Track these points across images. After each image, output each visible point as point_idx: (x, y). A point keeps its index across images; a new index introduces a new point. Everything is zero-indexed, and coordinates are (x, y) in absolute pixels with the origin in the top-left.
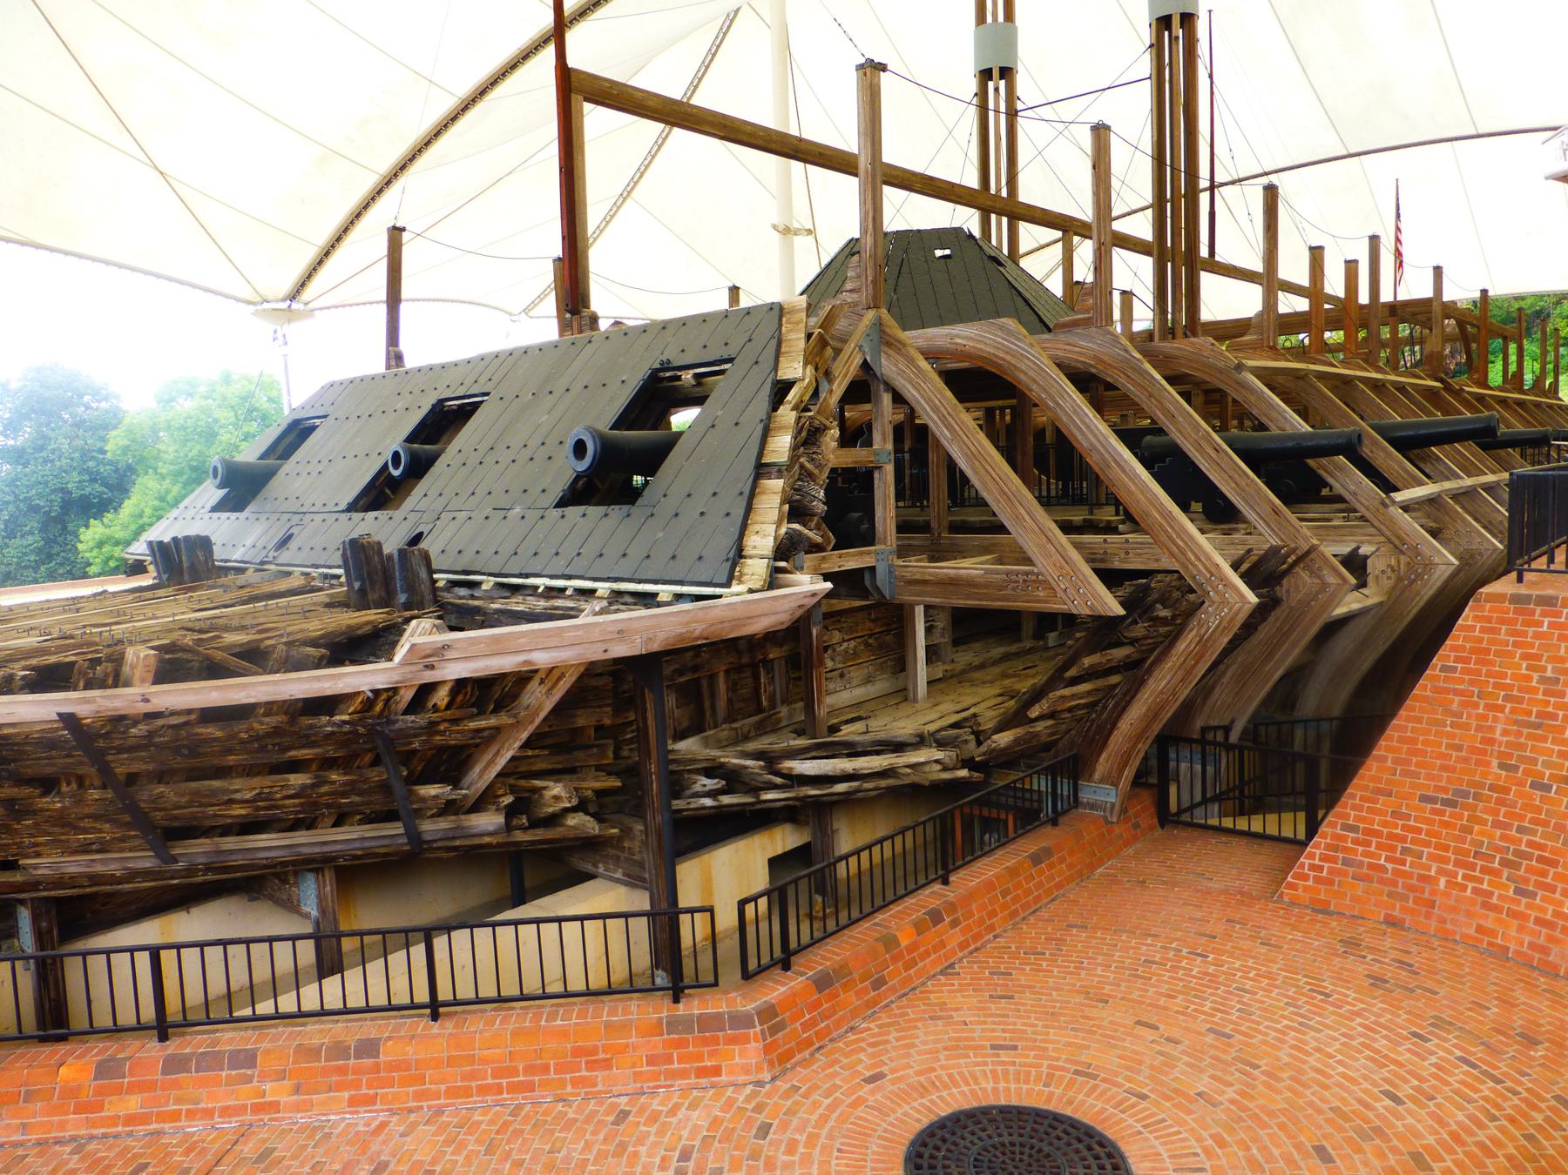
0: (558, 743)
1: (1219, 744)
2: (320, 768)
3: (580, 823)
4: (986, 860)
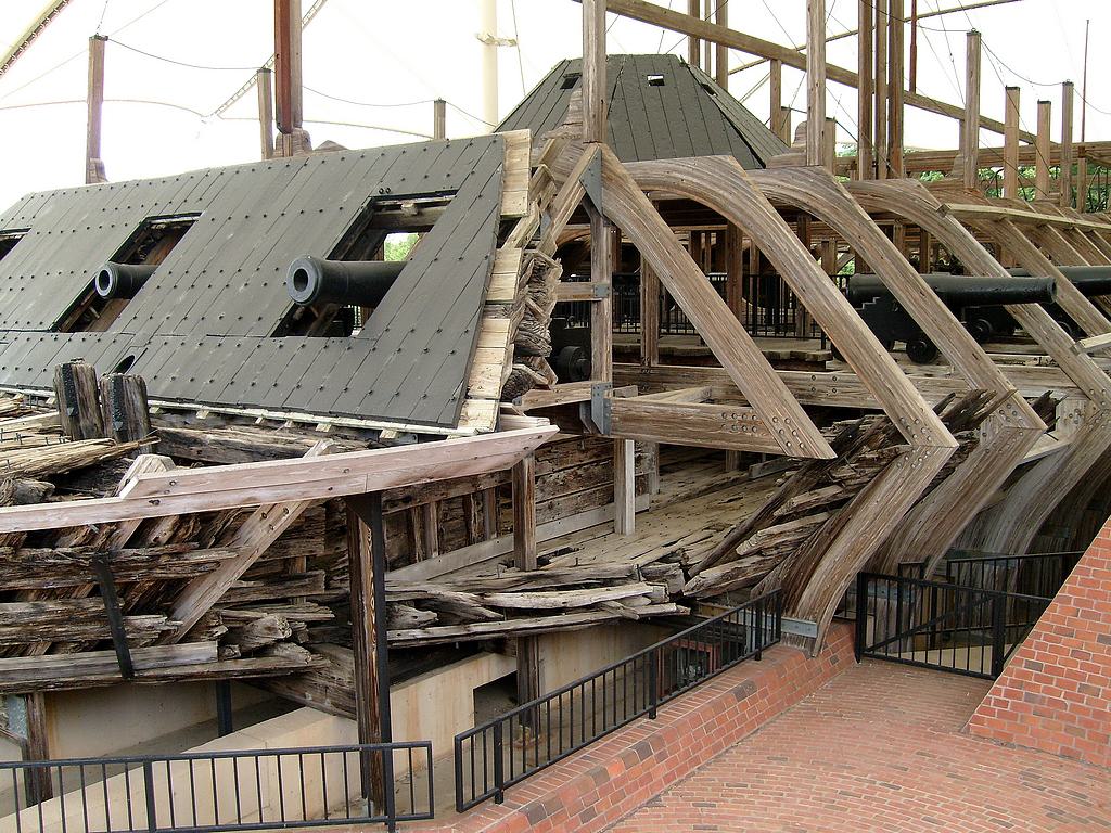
0: (274, 574)
1: (914, 581)
2: (38, 598)
3: (298, 655)
4: (691, 694)
